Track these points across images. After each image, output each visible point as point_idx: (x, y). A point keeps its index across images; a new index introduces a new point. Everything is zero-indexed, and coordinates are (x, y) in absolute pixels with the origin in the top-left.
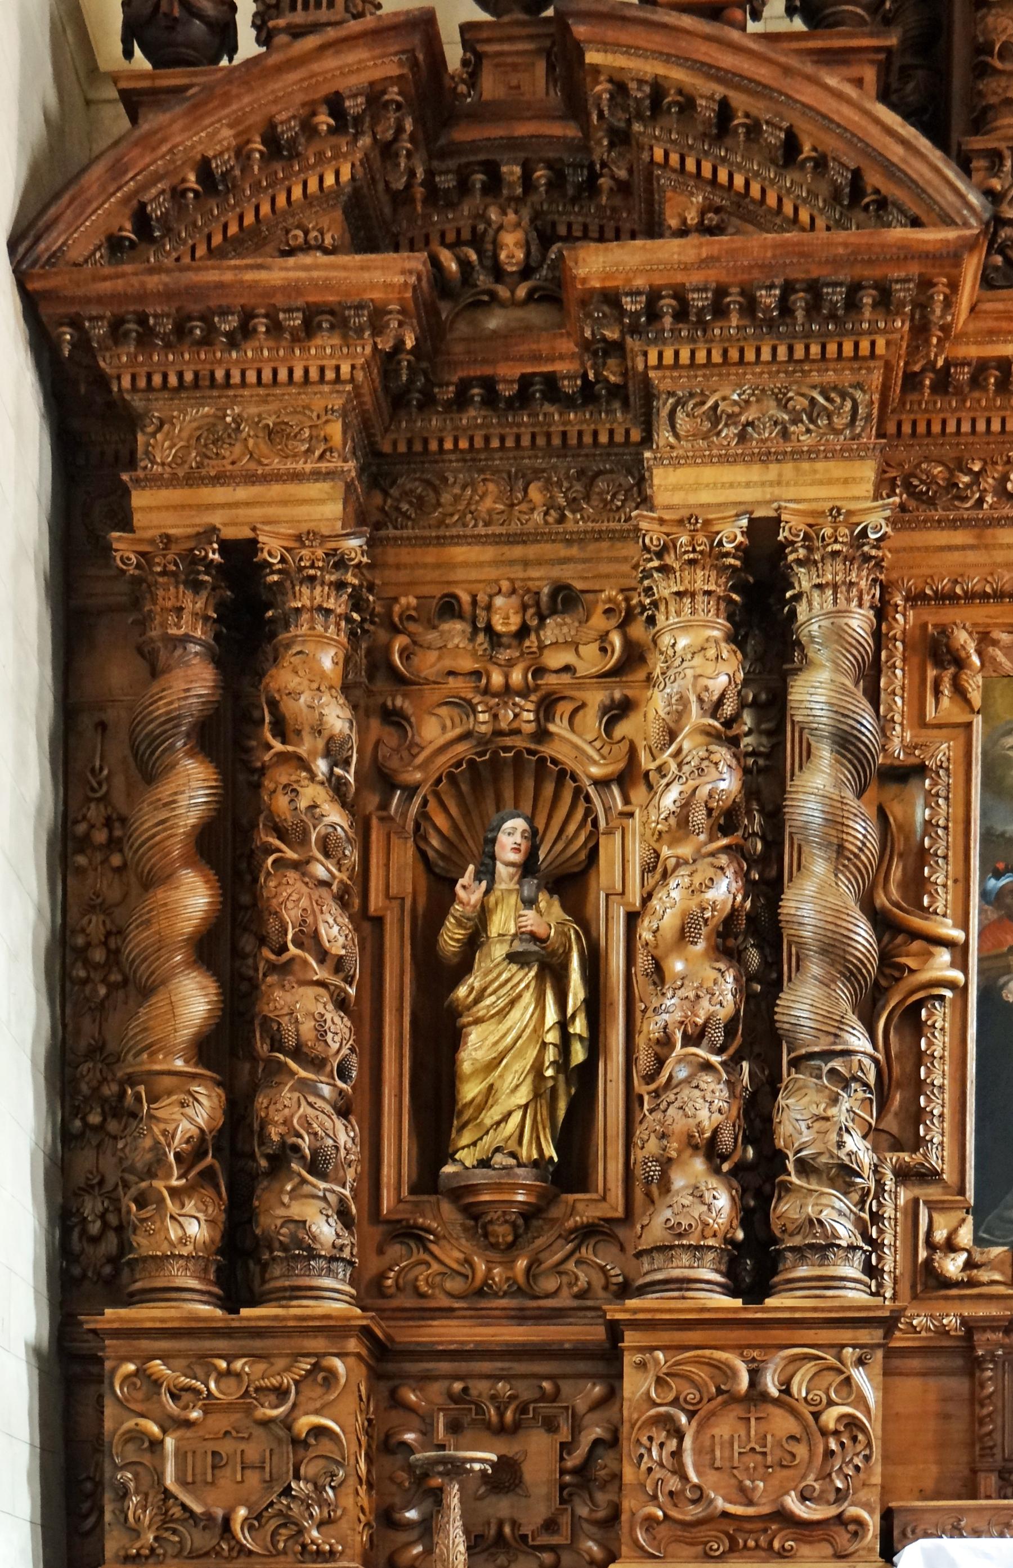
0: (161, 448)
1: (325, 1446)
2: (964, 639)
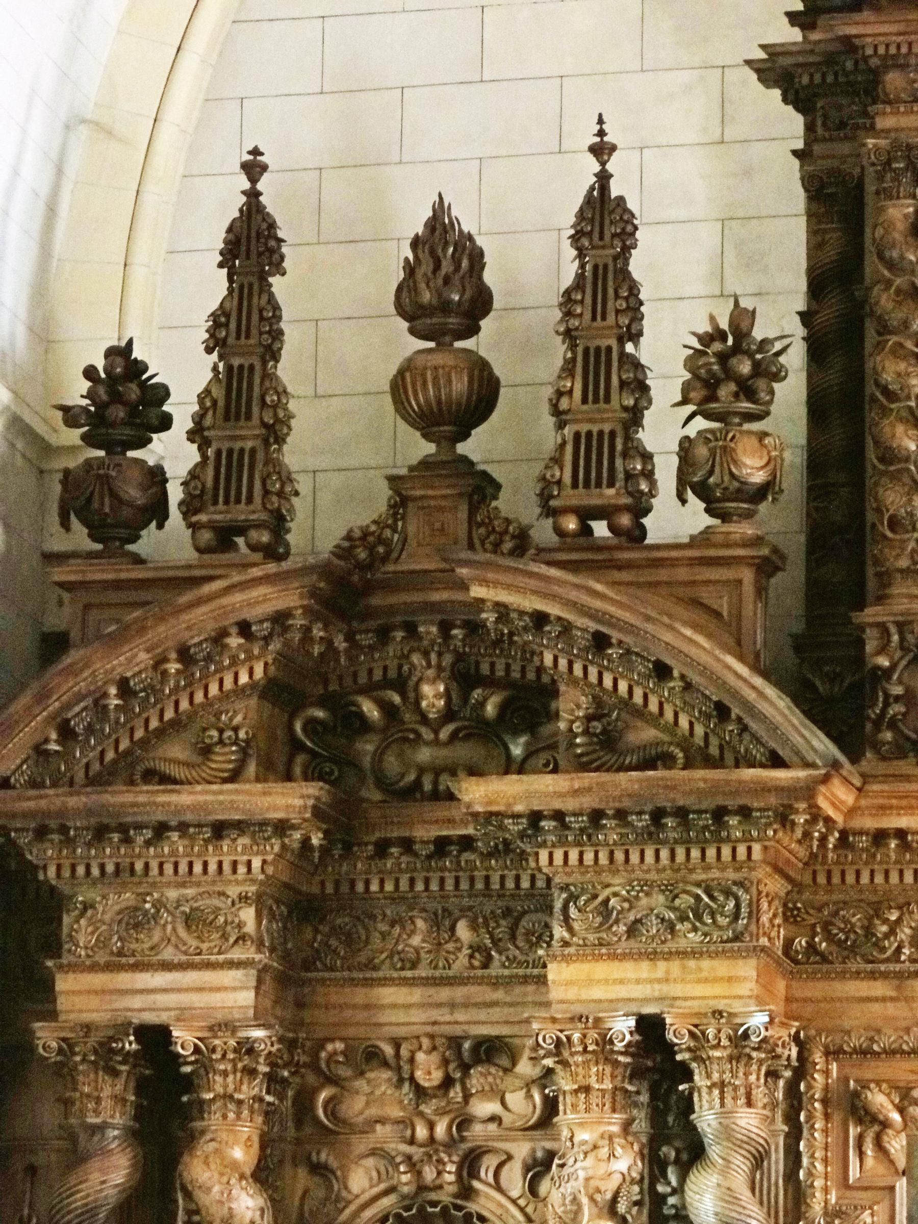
0: (81, 934)
2: (880, 1101)
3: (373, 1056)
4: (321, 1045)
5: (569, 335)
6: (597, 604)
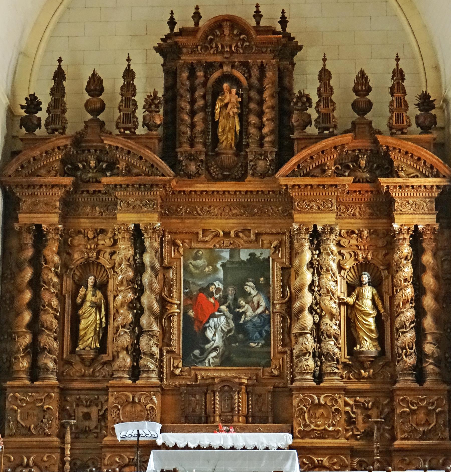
0: (24, 206)
1: (50, 412)
2: (179, 242)
3: (79, 232)
4: (70, 230)
5: (122, 95)
6: (129, 145)
